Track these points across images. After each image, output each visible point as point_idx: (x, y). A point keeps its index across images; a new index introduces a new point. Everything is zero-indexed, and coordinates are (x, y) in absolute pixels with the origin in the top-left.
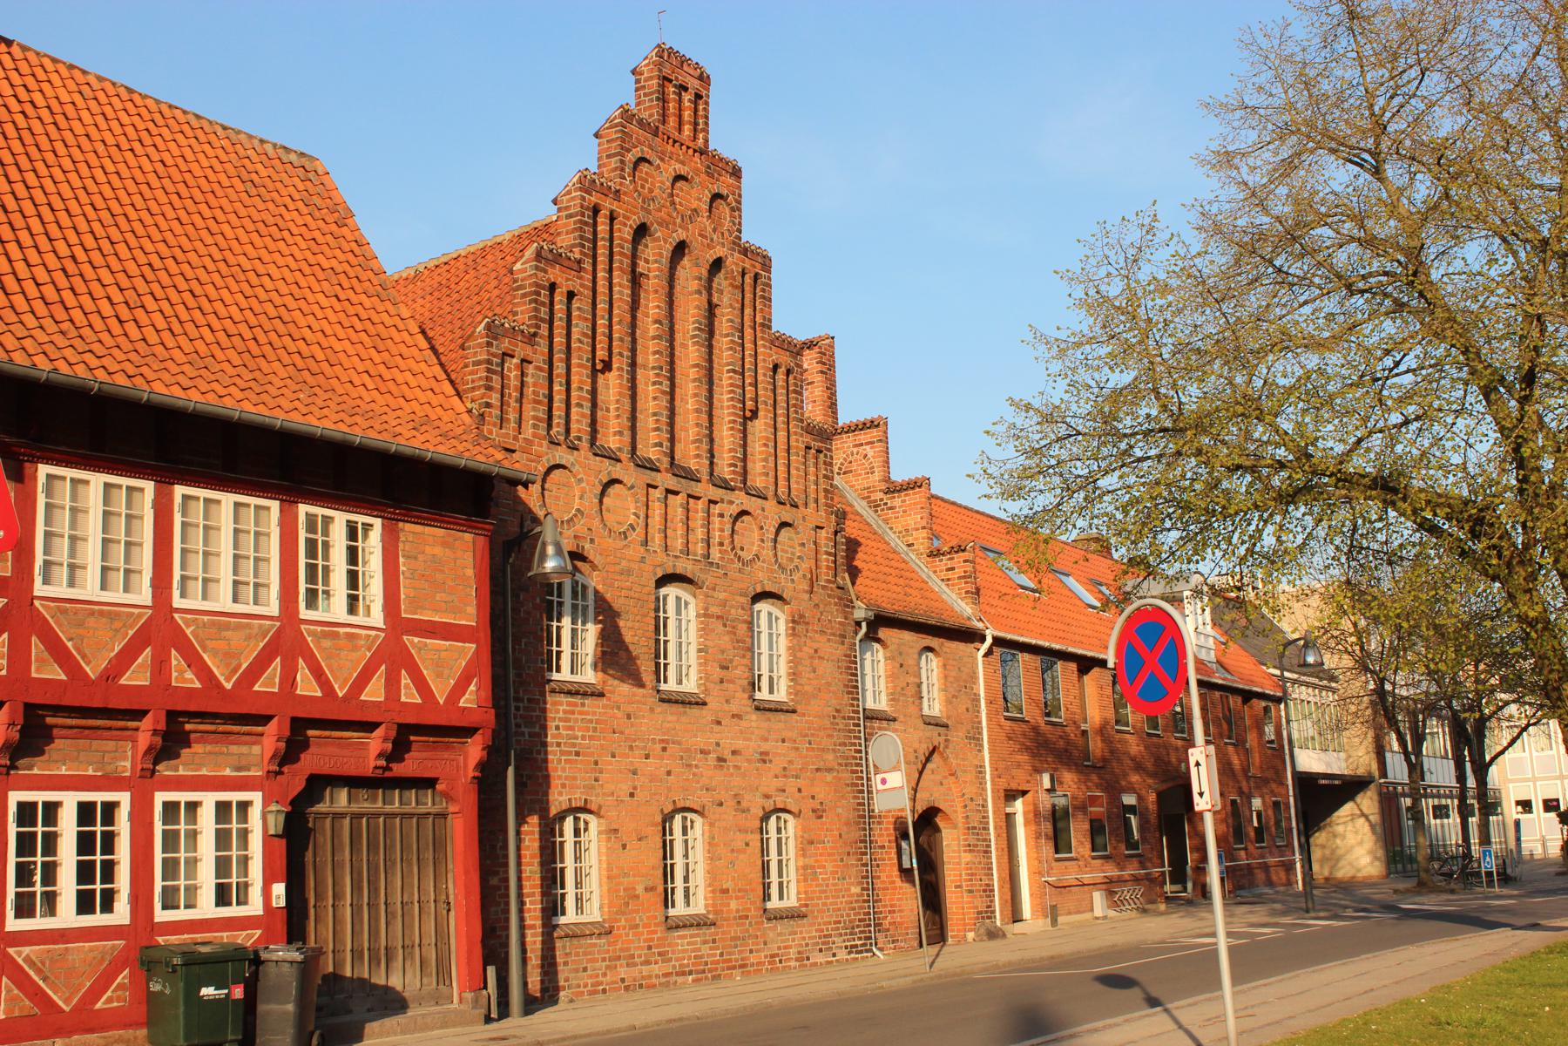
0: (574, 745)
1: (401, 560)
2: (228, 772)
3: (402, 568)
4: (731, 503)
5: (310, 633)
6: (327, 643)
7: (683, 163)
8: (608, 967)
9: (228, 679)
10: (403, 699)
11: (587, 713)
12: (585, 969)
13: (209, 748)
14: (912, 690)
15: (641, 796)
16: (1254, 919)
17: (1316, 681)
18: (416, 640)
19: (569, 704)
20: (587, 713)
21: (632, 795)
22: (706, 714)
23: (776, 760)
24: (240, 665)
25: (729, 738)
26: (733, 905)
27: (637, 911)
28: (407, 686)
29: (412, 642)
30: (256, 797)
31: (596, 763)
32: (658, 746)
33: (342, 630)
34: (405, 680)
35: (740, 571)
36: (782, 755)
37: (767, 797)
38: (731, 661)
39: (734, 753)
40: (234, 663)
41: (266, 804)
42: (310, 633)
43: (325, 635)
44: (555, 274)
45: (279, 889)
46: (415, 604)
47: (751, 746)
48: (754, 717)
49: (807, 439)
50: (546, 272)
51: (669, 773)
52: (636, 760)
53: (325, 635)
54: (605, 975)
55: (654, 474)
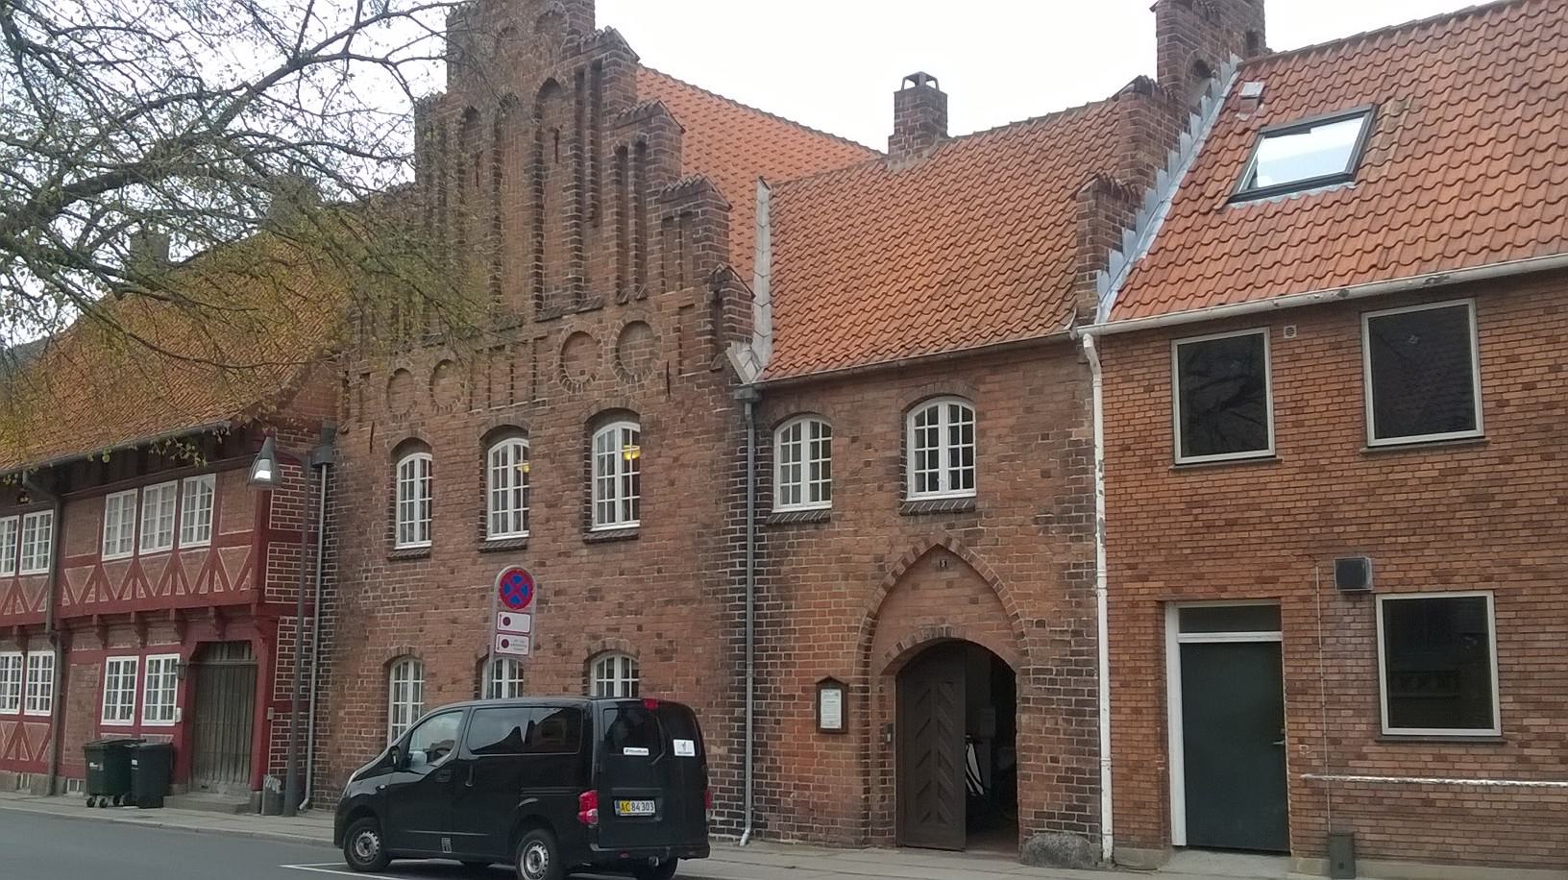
21: (449, 642)
37: (595, 637)
39: (557, 593)
48: (585, 552)
52: (456, 611)
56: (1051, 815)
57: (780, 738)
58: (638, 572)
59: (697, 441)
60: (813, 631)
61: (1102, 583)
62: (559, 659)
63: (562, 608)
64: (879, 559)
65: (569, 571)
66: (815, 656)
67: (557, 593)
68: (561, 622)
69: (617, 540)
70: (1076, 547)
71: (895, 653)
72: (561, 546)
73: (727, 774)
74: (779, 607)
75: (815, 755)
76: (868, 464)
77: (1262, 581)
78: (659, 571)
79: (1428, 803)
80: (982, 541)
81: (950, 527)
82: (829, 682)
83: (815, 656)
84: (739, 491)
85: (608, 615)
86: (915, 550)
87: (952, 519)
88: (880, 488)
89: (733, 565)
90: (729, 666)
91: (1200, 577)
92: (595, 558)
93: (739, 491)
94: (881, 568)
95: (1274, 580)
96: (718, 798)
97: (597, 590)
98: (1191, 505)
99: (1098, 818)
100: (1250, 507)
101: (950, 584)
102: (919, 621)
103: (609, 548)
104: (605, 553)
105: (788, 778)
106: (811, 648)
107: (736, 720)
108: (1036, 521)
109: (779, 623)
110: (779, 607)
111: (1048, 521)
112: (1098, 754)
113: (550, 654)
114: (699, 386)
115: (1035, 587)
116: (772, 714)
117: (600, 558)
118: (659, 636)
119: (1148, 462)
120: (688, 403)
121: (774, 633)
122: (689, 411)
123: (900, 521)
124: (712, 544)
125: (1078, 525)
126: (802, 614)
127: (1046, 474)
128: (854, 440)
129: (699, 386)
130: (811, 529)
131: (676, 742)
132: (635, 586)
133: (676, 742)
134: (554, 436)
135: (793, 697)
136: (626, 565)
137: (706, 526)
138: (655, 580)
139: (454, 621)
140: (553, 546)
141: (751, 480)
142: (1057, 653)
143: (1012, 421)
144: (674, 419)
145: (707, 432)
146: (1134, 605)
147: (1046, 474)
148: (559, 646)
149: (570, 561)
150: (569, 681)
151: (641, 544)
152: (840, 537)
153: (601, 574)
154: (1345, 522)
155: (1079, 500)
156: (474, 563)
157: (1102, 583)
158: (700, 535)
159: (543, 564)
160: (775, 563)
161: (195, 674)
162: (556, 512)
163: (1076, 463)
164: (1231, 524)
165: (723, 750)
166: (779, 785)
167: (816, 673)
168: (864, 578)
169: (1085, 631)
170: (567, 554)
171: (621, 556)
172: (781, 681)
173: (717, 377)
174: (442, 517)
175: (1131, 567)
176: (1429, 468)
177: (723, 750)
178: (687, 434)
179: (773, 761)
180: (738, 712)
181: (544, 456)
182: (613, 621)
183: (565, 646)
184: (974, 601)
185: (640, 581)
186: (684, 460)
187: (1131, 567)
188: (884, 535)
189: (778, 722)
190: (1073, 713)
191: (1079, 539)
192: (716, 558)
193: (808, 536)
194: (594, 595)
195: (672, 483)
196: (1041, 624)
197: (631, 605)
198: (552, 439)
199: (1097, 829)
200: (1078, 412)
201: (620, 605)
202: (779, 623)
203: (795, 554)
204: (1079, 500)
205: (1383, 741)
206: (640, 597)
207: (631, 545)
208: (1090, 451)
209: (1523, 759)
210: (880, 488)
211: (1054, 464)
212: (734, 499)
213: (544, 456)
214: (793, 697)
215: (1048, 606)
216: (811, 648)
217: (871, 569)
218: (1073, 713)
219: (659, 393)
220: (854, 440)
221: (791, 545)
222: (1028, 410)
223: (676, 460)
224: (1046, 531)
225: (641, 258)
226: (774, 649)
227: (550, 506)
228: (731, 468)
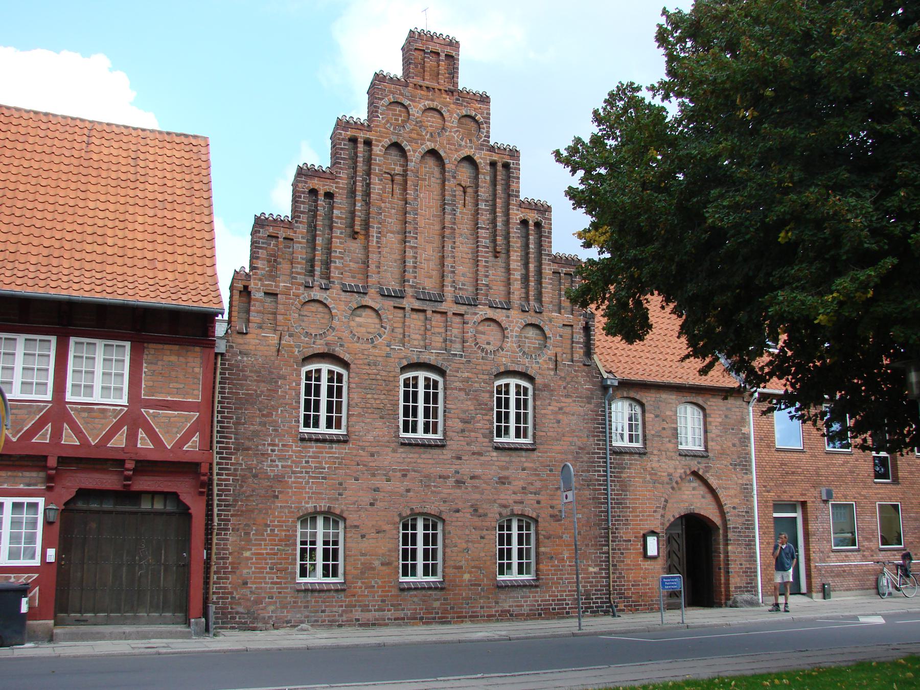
0: (321, 473)
1: (145, 365)
2: (21, 486)
3: (144, 370)
4: (476, 314)
5: (72, 409)
6: (85, 415)
7: (432, 100)
8: (343, 611)
9: (14, 436)
10: (139, 446)
11: (335, 453)
12: (323, 611)
13: (9, 473)
14: (669, 432)
15: (379, 505)
16: (325, 635)
17: (11, 463)
18: (151, 411)
19: (317, 447)
20: (335, 453)
21: (372, 504)
22: (447, 454)
23: (515, 483)
24: (22, 429)
25: (468, 467)
26: (466, 577)
27: (373, 578)
28: (142, 438)
29: (148, 413)
30: (41, 501)
31: (341, 484)
32: (399, 474)
33: (95, 407)
34: (141, 434)
35: (483, 358)
36: (519, 479)
37: (505, 506)
38: (473, 418)
39: (472, 478)
40: (18, 428)
41: (46, 503)
42: (72, 409)
43: (84, 410)
44: (315, 183)
45: (51, 554)
46: (151, 390)
47: (493, 472)
48: (495, 454)
49: (555, 267)
50: (306, 182)
51: (408, 491)
52: (379, 482)
53: (84, 410)
54: (341, 615)
55: (401, 300)
56: (741, 587)
57: (623, 561)
58: (536, 470)
59: (575, 401)
60: (638, 507)
61: (755, 492)
62: (476, 519)
63: (477, 487)
64: (670, 475)
65: (481, 464)
66: (641, 520)
67: (472, 478)
68: (478, 496)
69: (522, 449)
70: (745, 476)
71: (672, 519)
72: (474, 448)
73: (598, 582)
74: (621, 495)
75: (642, 569)
76: (664, 429)
77: (802, 495)
78: (551, 470)
79: (844, 571)
80: (712, 471)
81: (699, 463)
82: (653, 533)
83: (641, 520)
84: (601, 432)
85: (514, 493)
86: (685, 472)
87: (700, 460)
88: (670, 441)
89: (599, 471)
90: (599, 525)
91: (785, 492)
92: (503, 459)
93: (601, 432)
94: (671, 479)
95: (805, 495)
96: (594, 594)
97: (506, 478)
98: (782, 464)
99: (757, 586)
100: (799, 467)
101: (694, 489)
102: (682, 505)
103: (514, 454)
104: (511, 456)
105: (629, 581)
106: (638, 516)
107: (603, 553)
108: (731, 464)
109: (621, 503)
110: (621, 495)
111: (735, 465)
112: (756, 561)
113: (468, 516)
114: (575, 371)
115: (732, 492)
116: (619, 549)
117: (508, 459)
118: (552, 507)
119: (769, 446)
120: (568, 379)
121: (618, 508)
122: (568, 383)
123: (679, 458)
124: (585, 459)
125: (747, 470)
126: (633, 499)
127: (734, 445)
128: (657, 416)
129: (575, 371)
130: (636, 457)
131: (54, 550)
132: (535, 478)
133: (54, 550)
134: (469, 378)
135: (630, 541)
136: (526, 465)
137: (580, 448)
138: (548, 475)
139: (376, 490)
140: (467, 448)
141: (601, 425)
142: (741, 520)
143: (720, 420)
144: (559, 386)
145: (580, 397)
146: (766, 501)
147: (734, 445)
148: (476, 510)
149: (483, 458)
150: (485, 532)
151: (536, 453)
152: (653, 462)
153: (508, 468)
154: (821, 476)
155: (745, 458)
156: (394, 451)
157: (755, 492)
158: (577, 453)
159: (459, 458)
160: (618, 472)
161: (66, 529)
162: (470, 426)
163: (744, 442)
164: (793, 473)
165: (596, 569)
166: (624, 585)
167: (641, 529)
168: (662, 483)
169: (749, 512)
170: (480, 454)
171: (524, 459)
172: (624, 533)
173: (586, 368)
174: (359, 415)
175: (765, 486)
176: (840, 459)
177: (596, 569)
178: (567, 396)
179: (620, 573)
180: (605, 549)
181: (460, 390)
182: (518, 497)
183: (480, 511)
184: (703, 497)
185: (539, 475)
186: (567, 410)
187: (765, 486)
188: (672, 463)
189: (622, 554)
190: (747, 545)
191: (746, 474)
192: (588, 466)
193: (635, 460)
194: (503, 481)
195: (558, 422)
196: (734, 508)
197: (531, 488)
198: (467, 380)
199: (757, 591)
200: (743, 421)
201: (524, 488)
202: (621, 503)
203: (629, 468)
204: (745, 458)
205: (833, 551)
206: (538, 484)
207: (529, 453)
208: (749, 438)
209: (864, 556)
210: (670, 441)
211: (736, 441)
212: (598, 436)
213: (460, 390)
214: (630, 541)
215: (737, 501)
216: (638, 516)
217: (666, 479)
218: (747, 545)
219: (549, 369)
220: (657, 416)
221: (626, 464)
222: (726, 416)
223: (561, 409)
224: (735, 469)
225: (525, 279)
226: (619, 516)
227: (464, 421)
228: (596, 419)
